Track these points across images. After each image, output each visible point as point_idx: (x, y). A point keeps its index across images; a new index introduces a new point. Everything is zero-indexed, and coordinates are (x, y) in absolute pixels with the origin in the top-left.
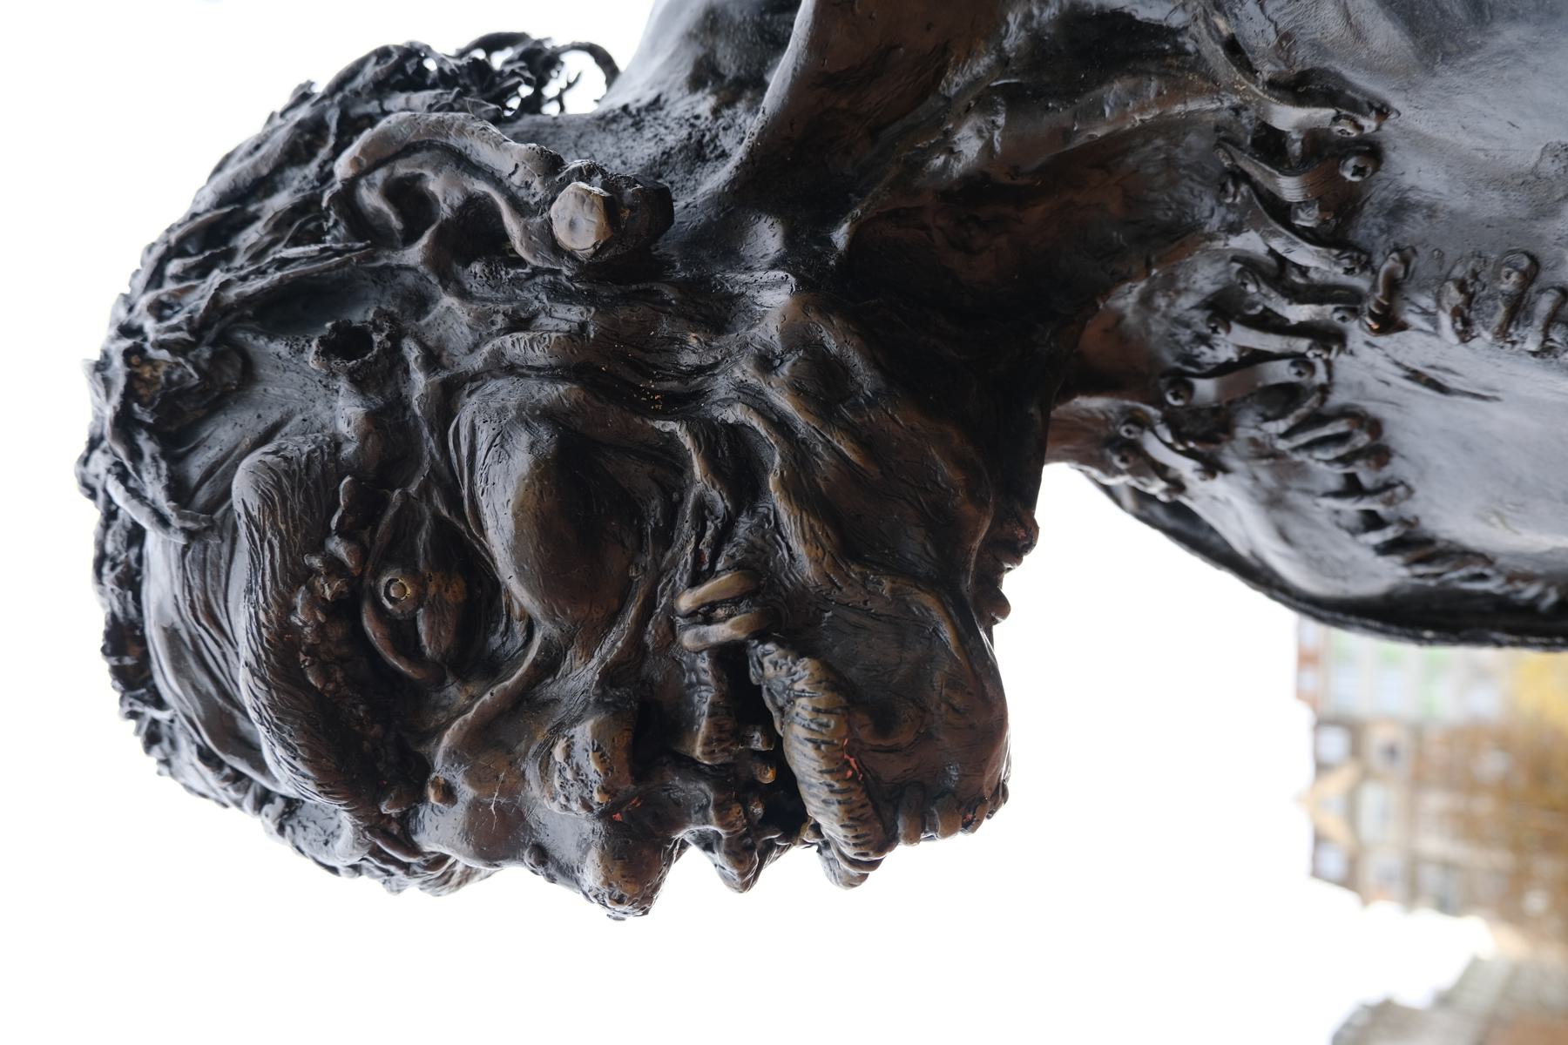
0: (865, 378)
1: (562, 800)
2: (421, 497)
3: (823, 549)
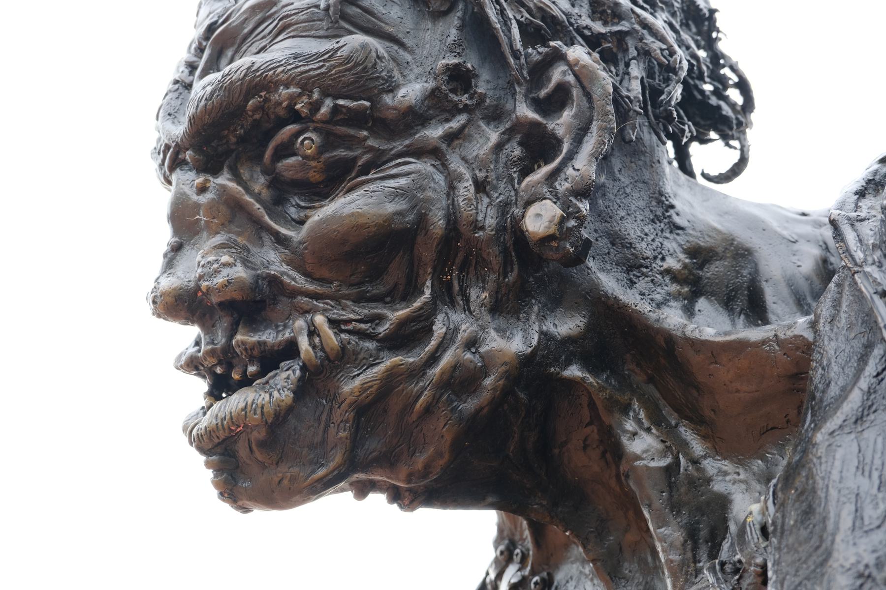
0: (469, 405)
1: (202, 263)
2: (366, 148)
3: (360, 395)
